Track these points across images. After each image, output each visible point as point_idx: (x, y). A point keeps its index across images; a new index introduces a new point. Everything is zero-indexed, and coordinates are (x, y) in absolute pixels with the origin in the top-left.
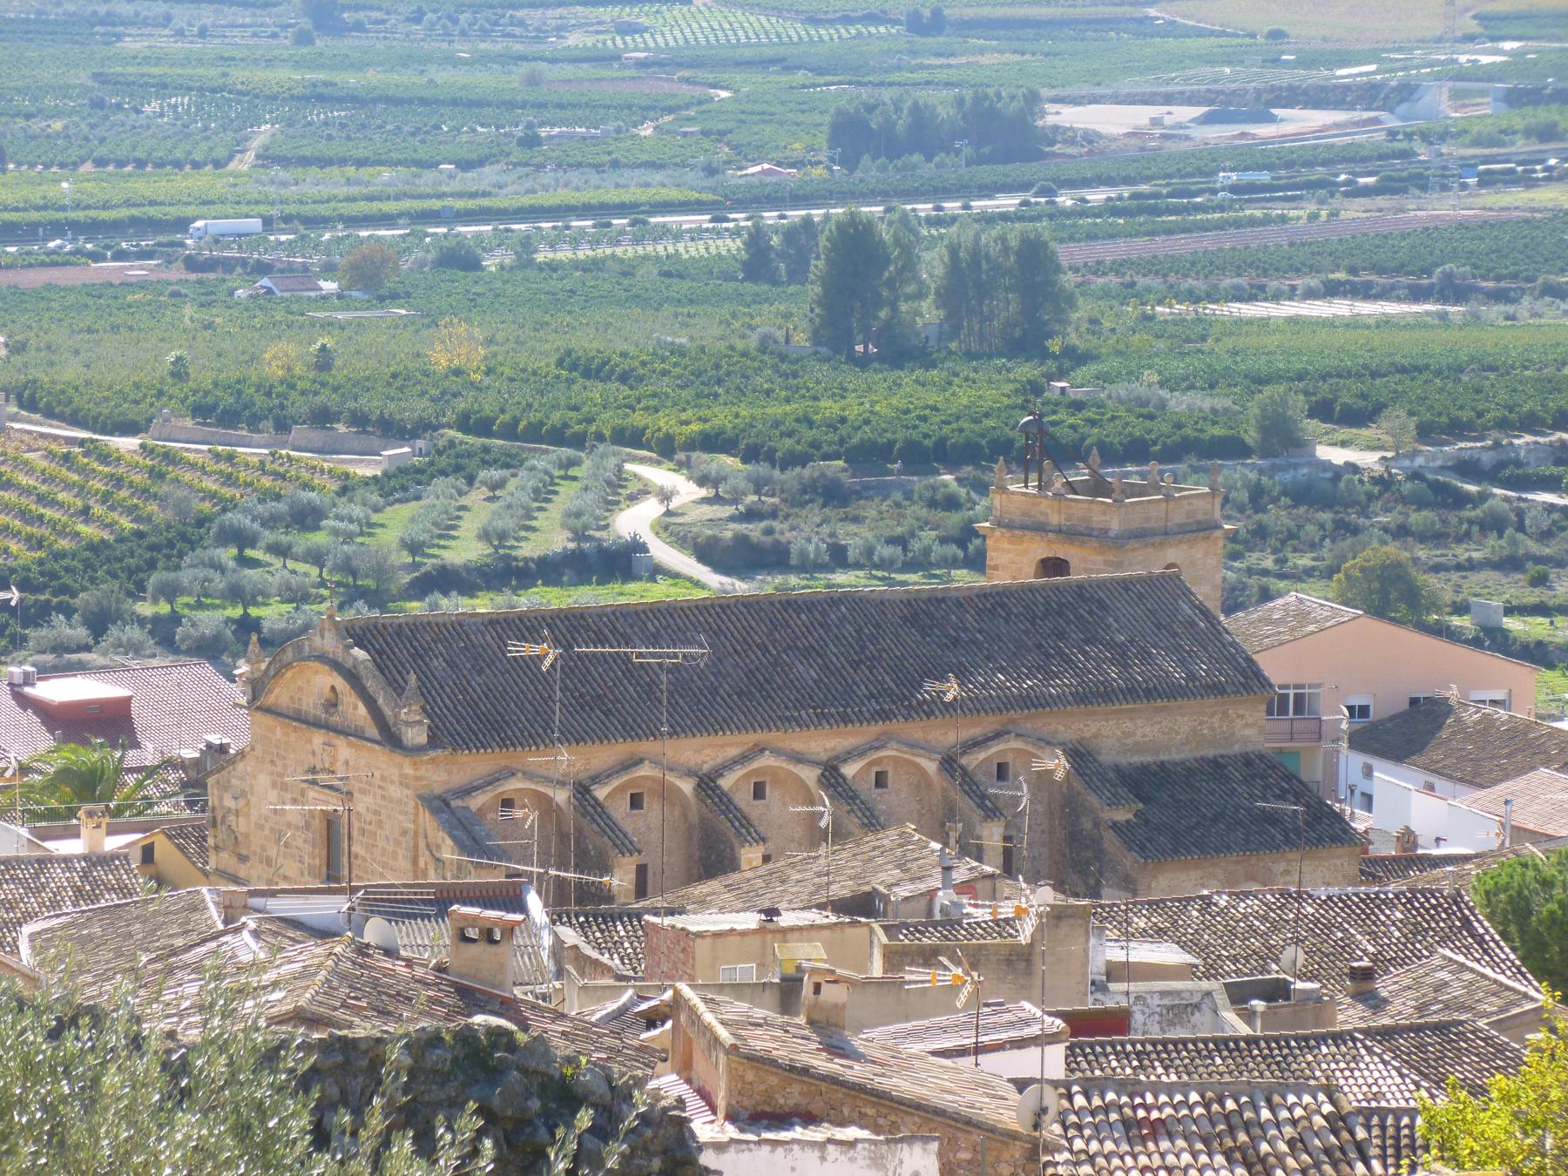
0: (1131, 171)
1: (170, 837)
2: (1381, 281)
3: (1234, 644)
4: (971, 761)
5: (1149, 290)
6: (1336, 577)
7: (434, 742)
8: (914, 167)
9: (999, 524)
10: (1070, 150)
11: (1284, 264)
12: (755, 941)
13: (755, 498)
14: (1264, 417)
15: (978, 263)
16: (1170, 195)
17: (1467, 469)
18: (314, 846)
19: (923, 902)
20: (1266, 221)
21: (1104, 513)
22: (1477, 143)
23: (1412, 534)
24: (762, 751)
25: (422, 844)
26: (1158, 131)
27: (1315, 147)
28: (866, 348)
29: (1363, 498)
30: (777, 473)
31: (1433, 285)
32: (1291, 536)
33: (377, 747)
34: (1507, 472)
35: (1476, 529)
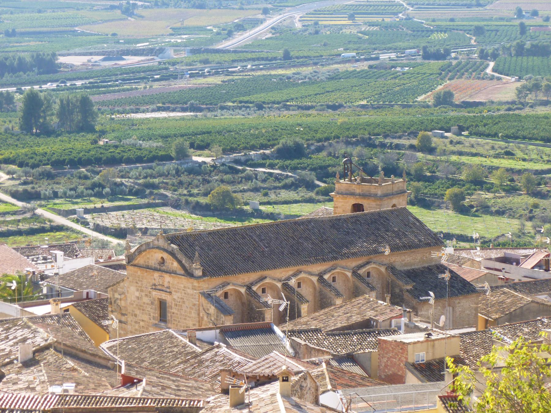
0: (87, 75)
1: (75, 307)
2: (173, 106)
3: (429, 229)
4: (362, 272)
5: (106, 111)
6: (209, 196)
7: (204, 275)
8: (21, 76)
9: (338, 193)
10: (65, 70)
11: (142, 102)
12: (425, 344)
13: (25, 178)
14: (177, 149)
15: (69, 105)
16: (100, 82)
17: (237, 162)
18: (155, 310)
19: (389, 321)
20: (132, 89)
21: (375, 189)
22: (187, 65)
23: (225, 182)
24: (301, 272)
25: (201, 308)
26: (91, 64)
27: (140, 67)
28: (36, 131)
29: (209, 171)
30: (31, 170)
31: (188, 107)
32: (190, 184)
33: (183, 277)
34: (250, 162)
35: (244, 180)
